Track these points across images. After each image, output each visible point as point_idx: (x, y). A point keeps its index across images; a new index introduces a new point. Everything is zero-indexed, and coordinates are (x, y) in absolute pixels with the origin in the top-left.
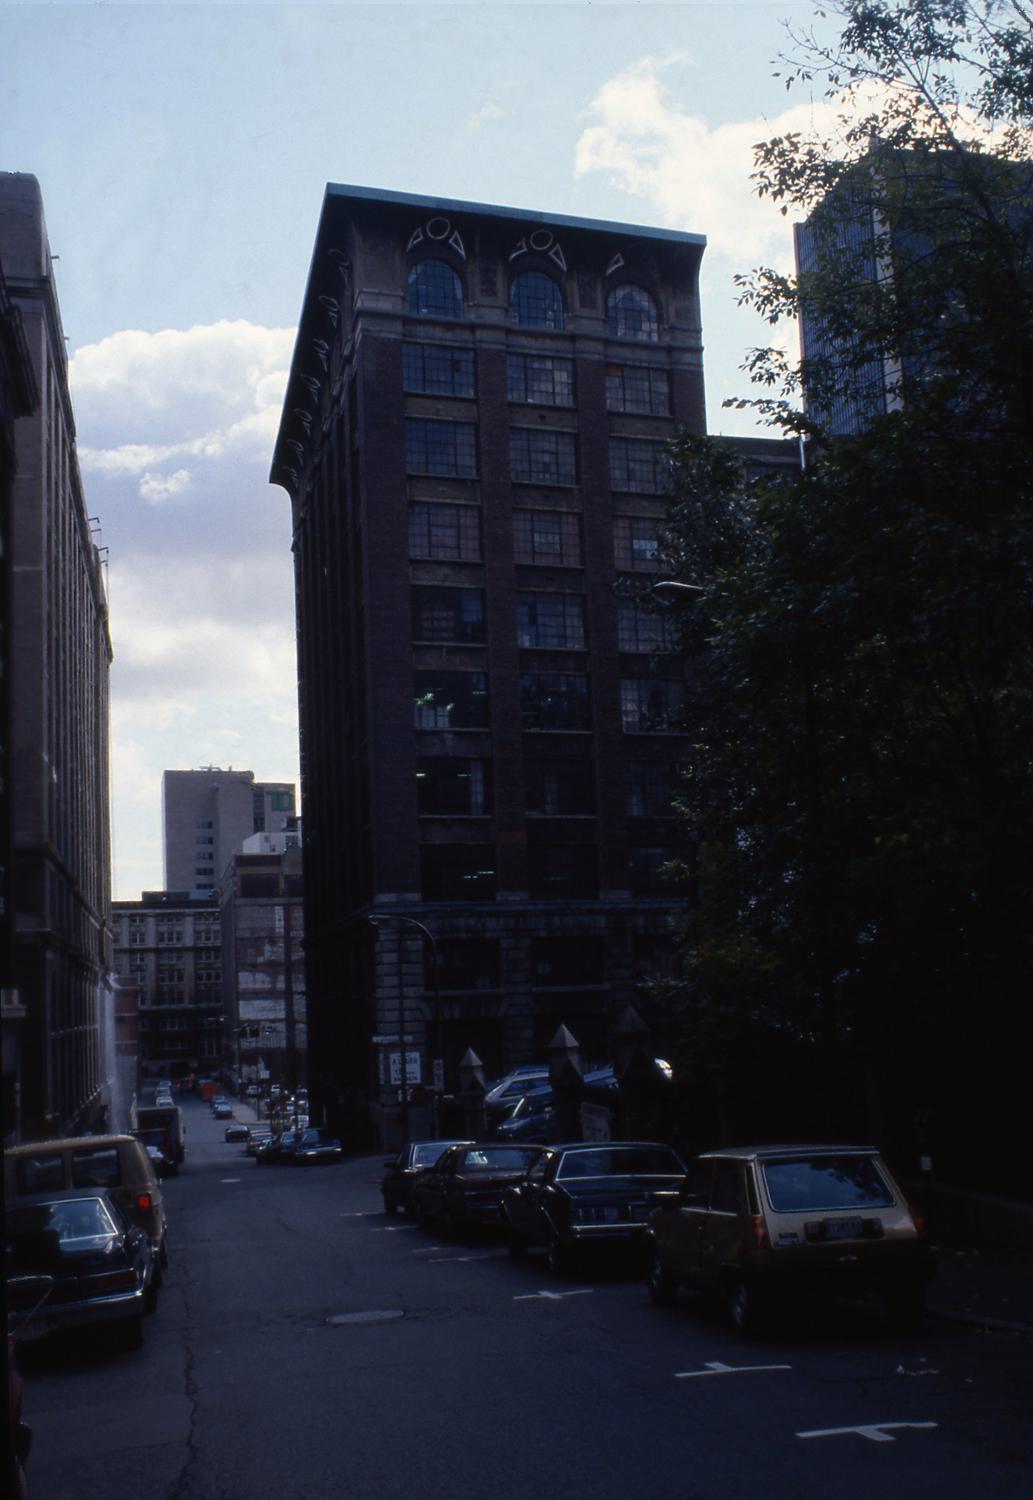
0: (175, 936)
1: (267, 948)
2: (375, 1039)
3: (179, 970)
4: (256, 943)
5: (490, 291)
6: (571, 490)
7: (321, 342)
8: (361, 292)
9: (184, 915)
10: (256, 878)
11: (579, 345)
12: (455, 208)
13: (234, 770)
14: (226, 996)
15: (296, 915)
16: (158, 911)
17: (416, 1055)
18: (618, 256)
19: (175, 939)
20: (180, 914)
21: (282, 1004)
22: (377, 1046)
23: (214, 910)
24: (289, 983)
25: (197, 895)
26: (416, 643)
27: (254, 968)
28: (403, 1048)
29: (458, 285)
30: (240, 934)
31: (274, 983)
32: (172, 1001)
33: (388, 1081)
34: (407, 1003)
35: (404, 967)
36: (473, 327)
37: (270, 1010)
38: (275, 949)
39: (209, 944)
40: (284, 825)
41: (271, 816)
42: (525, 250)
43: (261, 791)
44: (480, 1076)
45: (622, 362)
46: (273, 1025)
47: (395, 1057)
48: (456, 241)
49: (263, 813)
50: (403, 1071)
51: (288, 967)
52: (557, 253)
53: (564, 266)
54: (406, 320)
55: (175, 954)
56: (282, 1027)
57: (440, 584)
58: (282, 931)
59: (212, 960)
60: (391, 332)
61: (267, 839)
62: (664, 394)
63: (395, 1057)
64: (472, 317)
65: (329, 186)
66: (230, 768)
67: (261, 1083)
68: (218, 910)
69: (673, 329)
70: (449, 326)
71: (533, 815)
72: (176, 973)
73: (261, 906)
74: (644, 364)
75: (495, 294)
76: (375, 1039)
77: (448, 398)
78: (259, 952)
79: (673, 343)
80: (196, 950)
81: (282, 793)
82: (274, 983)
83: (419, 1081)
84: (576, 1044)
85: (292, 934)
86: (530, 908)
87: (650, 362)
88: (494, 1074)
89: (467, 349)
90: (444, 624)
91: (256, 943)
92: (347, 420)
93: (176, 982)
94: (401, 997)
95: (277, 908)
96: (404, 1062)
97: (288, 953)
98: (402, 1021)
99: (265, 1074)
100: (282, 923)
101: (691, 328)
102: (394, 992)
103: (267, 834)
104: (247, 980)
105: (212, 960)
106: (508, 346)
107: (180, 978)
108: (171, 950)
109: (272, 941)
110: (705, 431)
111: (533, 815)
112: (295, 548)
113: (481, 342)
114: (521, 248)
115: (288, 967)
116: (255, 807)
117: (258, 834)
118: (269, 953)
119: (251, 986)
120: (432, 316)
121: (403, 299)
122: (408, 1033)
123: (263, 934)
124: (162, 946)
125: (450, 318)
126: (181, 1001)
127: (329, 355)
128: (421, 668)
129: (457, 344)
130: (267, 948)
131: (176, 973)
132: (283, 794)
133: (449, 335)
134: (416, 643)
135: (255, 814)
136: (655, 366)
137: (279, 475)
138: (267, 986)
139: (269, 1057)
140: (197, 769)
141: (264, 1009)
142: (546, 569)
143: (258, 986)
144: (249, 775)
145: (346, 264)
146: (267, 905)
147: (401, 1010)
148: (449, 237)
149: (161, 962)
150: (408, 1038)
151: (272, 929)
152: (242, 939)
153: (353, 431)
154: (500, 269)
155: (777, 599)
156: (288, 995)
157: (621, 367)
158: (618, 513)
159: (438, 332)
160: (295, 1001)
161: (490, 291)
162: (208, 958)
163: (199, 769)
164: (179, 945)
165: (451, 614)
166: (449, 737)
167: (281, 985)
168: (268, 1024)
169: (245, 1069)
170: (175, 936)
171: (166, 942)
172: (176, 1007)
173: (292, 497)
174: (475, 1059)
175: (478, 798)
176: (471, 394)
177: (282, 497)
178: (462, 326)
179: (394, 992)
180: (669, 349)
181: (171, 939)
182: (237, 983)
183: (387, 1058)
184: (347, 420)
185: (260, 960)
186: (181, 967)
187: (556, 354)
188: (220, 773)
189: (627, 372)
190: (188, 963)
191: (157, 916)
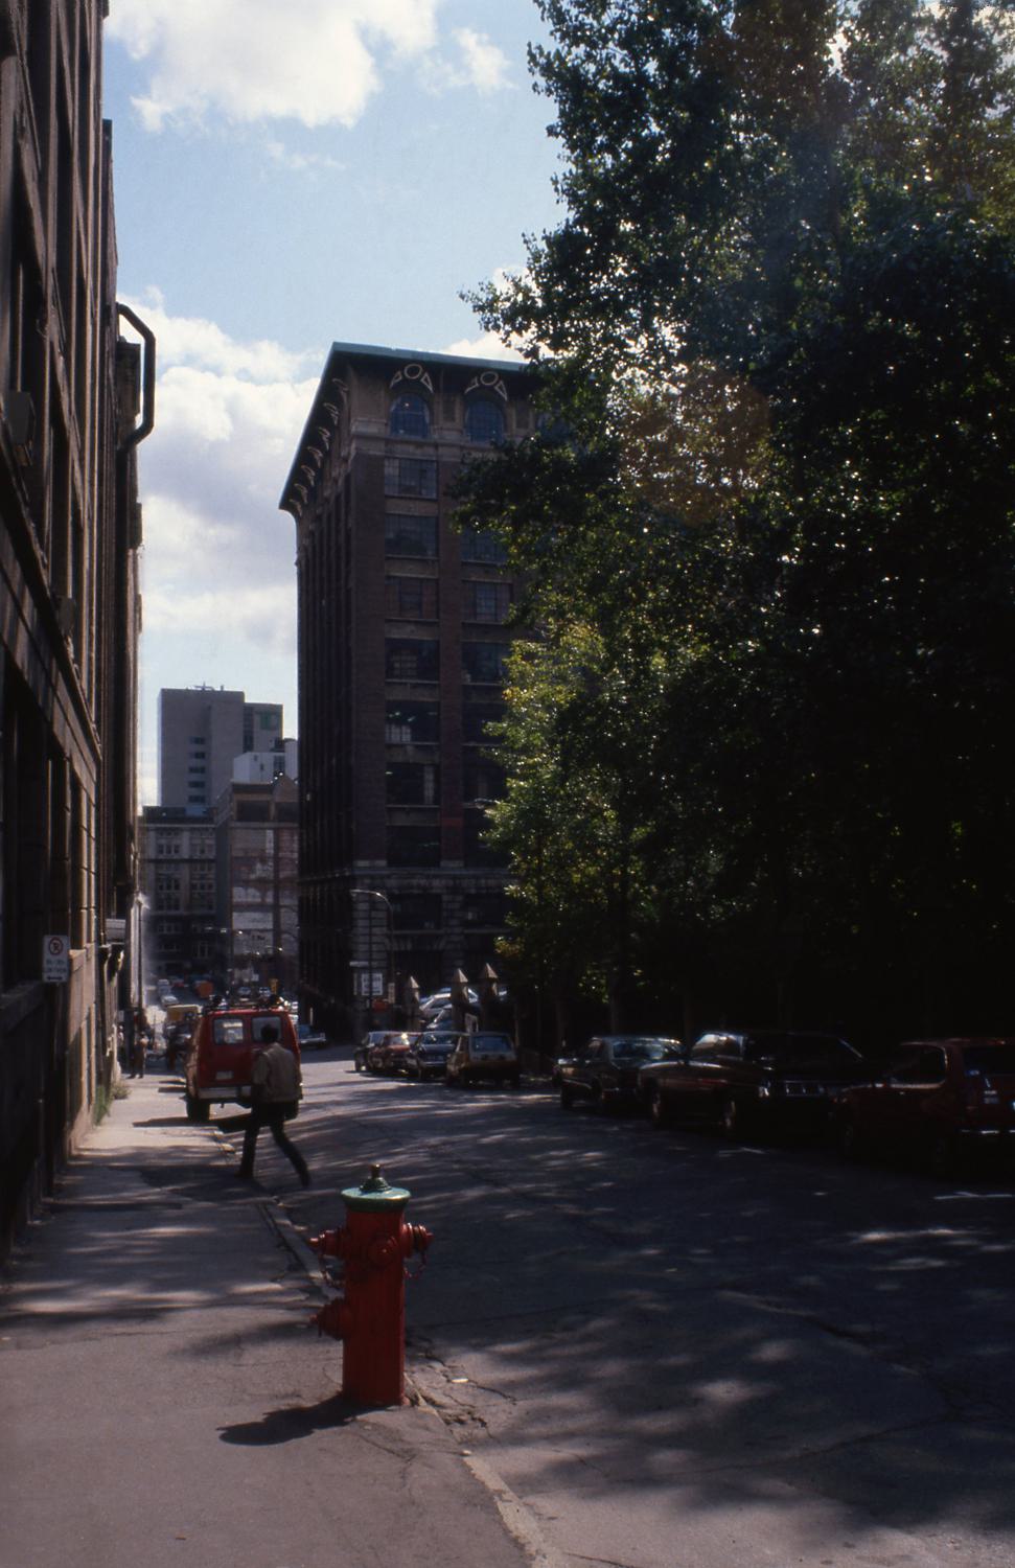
0: (173, 849)
1: (259, 866)
2: (352, 963)
3: (176, 881)
4: (248, 862)
5: (450, 417)
7: (325, 430)
8: (356, 421)
9: (182, 830)
10: (251, 807)
13: (225, 689)
14: (222, 911)
15: (285, 838)
16: (159, 825)
17: (380, 975)
19: (173, 852)
20: (177, 828)
21: (270, 917)
23: (209, 826)
24: (276, 897)
25: (196, 810)
26: (389, 680)
27: (246, 884)
28: (370, 970)
29: (427, 413)
30: (235, 854)
31: (263, 897)
32: (169, 908)
33: (360, 993)
34: (375, 939)
35: (374, 914)
36: (436, 446)
37: (258, 921)
38: (265, 868)
39: (204, 857)
40: (272, 745)
41: (259, 735)
42: (477, 385)
43: (252, 710)
44: (417, 995)
46: (262, 935)
47: (365, 976)
48: (426, 380)
49: (252, 732)
50: (370, 987)
51: (277, 885)
54: (387, 441)
55: (173, 866)
56: (269, 936)
58: (272, 852)
59: (206, 872)
60: (376, 450)
61: (256, 758)
63: (365, 976)
64: (436, 437)
65: (335, 344)
66: (222, 687)
67: (250, 985)
68: (213, 826)
70: (419, 445)
72: (173, 882)
73: (255, 829)
75: (453, 419)
76: (352, 963)
77: (416, 499)
78: (252, 871)
80: (190, 861)
81: (272, 714)
83: (381, 994)
84: (496, 977)
85: (281, 855)
86: (464, 872)
88: (425, 992)
89: (432, 461)
90: (409, 665)
91: (248, 862)
92: (343, 498)
93: (173, 890)
95: (268, 831)
96: (371, 980)
97: (276, 871)
98: (370, 951)
100: (272, 845)
102: (367, 931)
103: (258, 754)
104: (239, 895)
105: (206, 872)
107: (177, 887)
108: (170, 861)
109: (263, 861)
110: (304, 1062)
112: (298, 563)
115: (277, 885)
116: (245, 726)
117: (248, 754)
118: (260, 871)
119: (244, 900)
120: (407, 437)
121: (386, 425)
122: (376, 960)
123: (254, 855)
124: (161, 857)
125: (419, 438)
126: (177, 908)
127: (330, 439)
128: (391, 698)
129: (425, 458)
130: (259, 866)
131: (173, 882)
133: (418, 451)
134: (389, 680)
135: (245, 732)
137: (286, 504)
138: (259, 900)
139: (258, 964)
140: (192, 687)
141: (254, 920)
143: (250, 900)
144: (241, 695)
145: (346, 389)
146: (261, 829)
148: (421, 377)
149: (160, 872)
150: (375, 964)
151: (263, 850)
152: (237, 858)
153: (347, 514)
154: (458, 400)
156: (276, 908)
159: (411, 448)
160: (282, 915)
161: (450, 417)
162: (202, 869)
163: (194, 688)
164: (176, 857)
165: (415, 658)
166: (410, 748)
167: (270, 900)
168: (259, 934)
169: (237, 973)
170: (173, 849)
171: (165, 854)
172: (173, 912)
173: (293, 514)
174: (415, 984)
175: (429, 790)
176: (434, 496)
177: (288, 520)
178: (429, 445)
181: (169, 852)
182: (231, 897)
183: (359, 977)
184: (343, 498)
185: (253, 877)
186: (177, 876)
188: (213, 693)
190: (184, 874)
191: (157, 829)
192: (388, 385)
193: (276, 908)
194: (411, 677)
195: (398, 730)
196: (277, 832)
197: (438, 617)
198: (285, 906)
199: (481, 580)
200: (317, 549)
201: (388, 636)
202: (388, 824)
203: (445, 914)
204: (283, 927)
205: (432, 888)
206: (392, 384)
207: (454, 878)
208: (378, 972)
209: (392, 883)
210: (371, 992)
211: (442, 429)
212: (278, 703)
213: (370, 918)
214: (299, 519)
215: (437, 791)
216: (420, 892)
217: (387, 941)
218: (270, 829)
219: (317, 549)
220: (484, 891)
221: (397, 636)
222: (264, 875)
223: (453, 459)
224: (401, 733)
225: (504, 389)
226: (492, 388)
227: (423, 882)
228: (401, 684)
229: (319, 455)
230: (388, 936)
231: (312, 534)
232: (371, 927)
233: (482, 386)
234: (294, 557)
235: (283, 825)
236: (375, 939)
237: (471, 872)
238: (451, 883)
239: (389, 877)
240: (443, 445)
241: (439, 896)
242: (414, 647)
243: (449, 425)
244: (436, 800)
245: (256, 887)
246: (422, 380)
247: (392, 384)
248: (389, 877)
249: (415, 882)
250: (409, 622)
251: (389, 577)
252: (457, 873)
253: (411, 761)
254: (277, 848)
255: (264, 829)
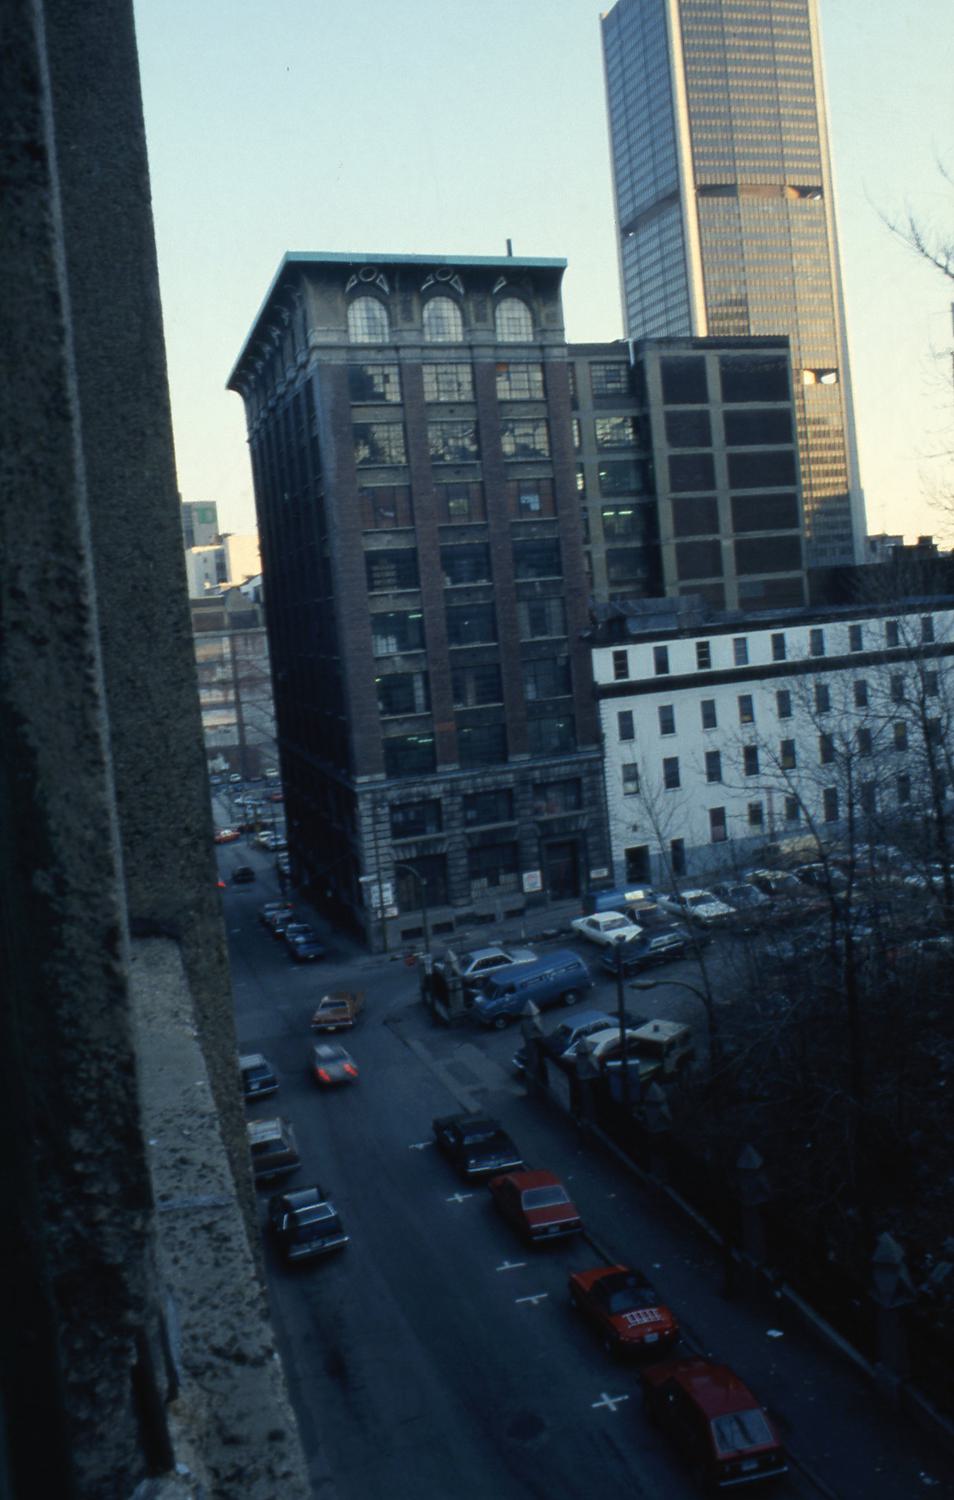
1: (219, 670)
6: (474, 465)
11: (476, 352)
12: (380, 261)
18: (502, 278)
21: (233, 713)
22: (366, 883)
24: (237, 695)
26: (372, 593)
27: (210, 686)
31: (226, 696)
34: (381, 851)
35: (378, 827)
38: (225, 670)
45: (507, 361)
47: (375, 888)
52: (456, 282)
53: (462, 291)
56: (234, 729)
57: (385, 548)
62: (538, 381)
69: (544, 331)
71: (459, 707)
74: (524, 361)
76: (362, 879)
78: (213, 673)
79: (545, 343)
82: (226, 696)
85: (238, 658)
86: (461, 775)
87: (528, 358)
91: (210, 665)
94: (377, 848)
96: (381, 891)
97: (235, 672)
99: (225, 766)
101: (557, 328)
102: (372, 844)
106: (425, 359)
111: (459, 707)
113: (404, 359)
114: (430, 280)
118: (221, 673)
128: (375, 612)
130: (219, 670)
132: (207, 509)
133: (380, 356)
134: (372, 593)
136: (531, 361)
137: (235, 383)
142: (460, 527)
143: (214, 699)
147: (377, 856)
148: (376, 278)
155: (645, 1032)
157: (507, 364)
158: (510, 478)
160: (243, 709)
165: (393, 567)
167: (232, 697)
177: (236, 400)
179: (372, 844)
180: (542, 348)
185: (214, 679)
187: (458, 361)
189: (511, 368)
192: (344, 291)
193: (238, 704)
194: (392, 586)
195: (384, 642)
196: (232, 638)
197: (413, 524)
198: (248, 702)
199: (452, 481)
200: (273, 436)
201: (366, 549)
202: (382, 737)
203: (445, 817)
204: (246, 721)
205: (430, 794)
206: (348, 288)
207: (452, 781)
208: (387, 882)
209: (392, 794)
210: (382, 902)
211: (401, 331)
212: (212, 499)
213: (374, 832)
214: (247, 400)
215: (428, 697)
216: (420, 799)
217: (392, 851)
218: (225, 636)
219: (273, 436)
220: (481, 790)
221: (374, 548)
222: (225, 677)
223: (415, 361)
224: (388, 645)
225: (460, 283)
226: (447, 283)
227: (421, 789)
228: (382, 595)
229: (267, 348)
230: (395, 847)
231: (265, 421)
232: (376, 839)
233: (437, 282)
234: (245, 436)
235: (237, 631)
236: (381, 851)
237: (468, 774)
238: (448, 786)
239: (389, 789)
240: (405, 347)
241: (437, 802)
242: (392, 556)
243: (407, 326)
244: (428, 707)
245: (219, 688)
246: (378, 281)
247: (348, 288)
248: (389, 789)
249: (414, 790)
250: (386, 532)
251: (363, 489)
252: (454, 776)
253: (400, 672)
254: (234, 652)
255: (222, 636)
